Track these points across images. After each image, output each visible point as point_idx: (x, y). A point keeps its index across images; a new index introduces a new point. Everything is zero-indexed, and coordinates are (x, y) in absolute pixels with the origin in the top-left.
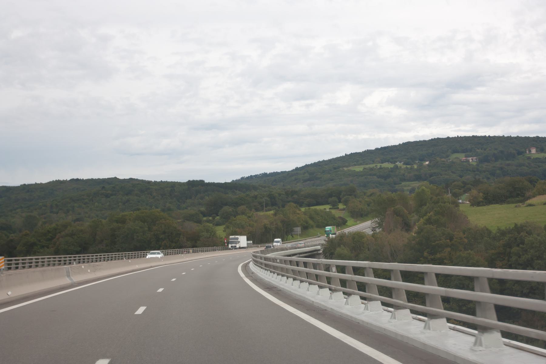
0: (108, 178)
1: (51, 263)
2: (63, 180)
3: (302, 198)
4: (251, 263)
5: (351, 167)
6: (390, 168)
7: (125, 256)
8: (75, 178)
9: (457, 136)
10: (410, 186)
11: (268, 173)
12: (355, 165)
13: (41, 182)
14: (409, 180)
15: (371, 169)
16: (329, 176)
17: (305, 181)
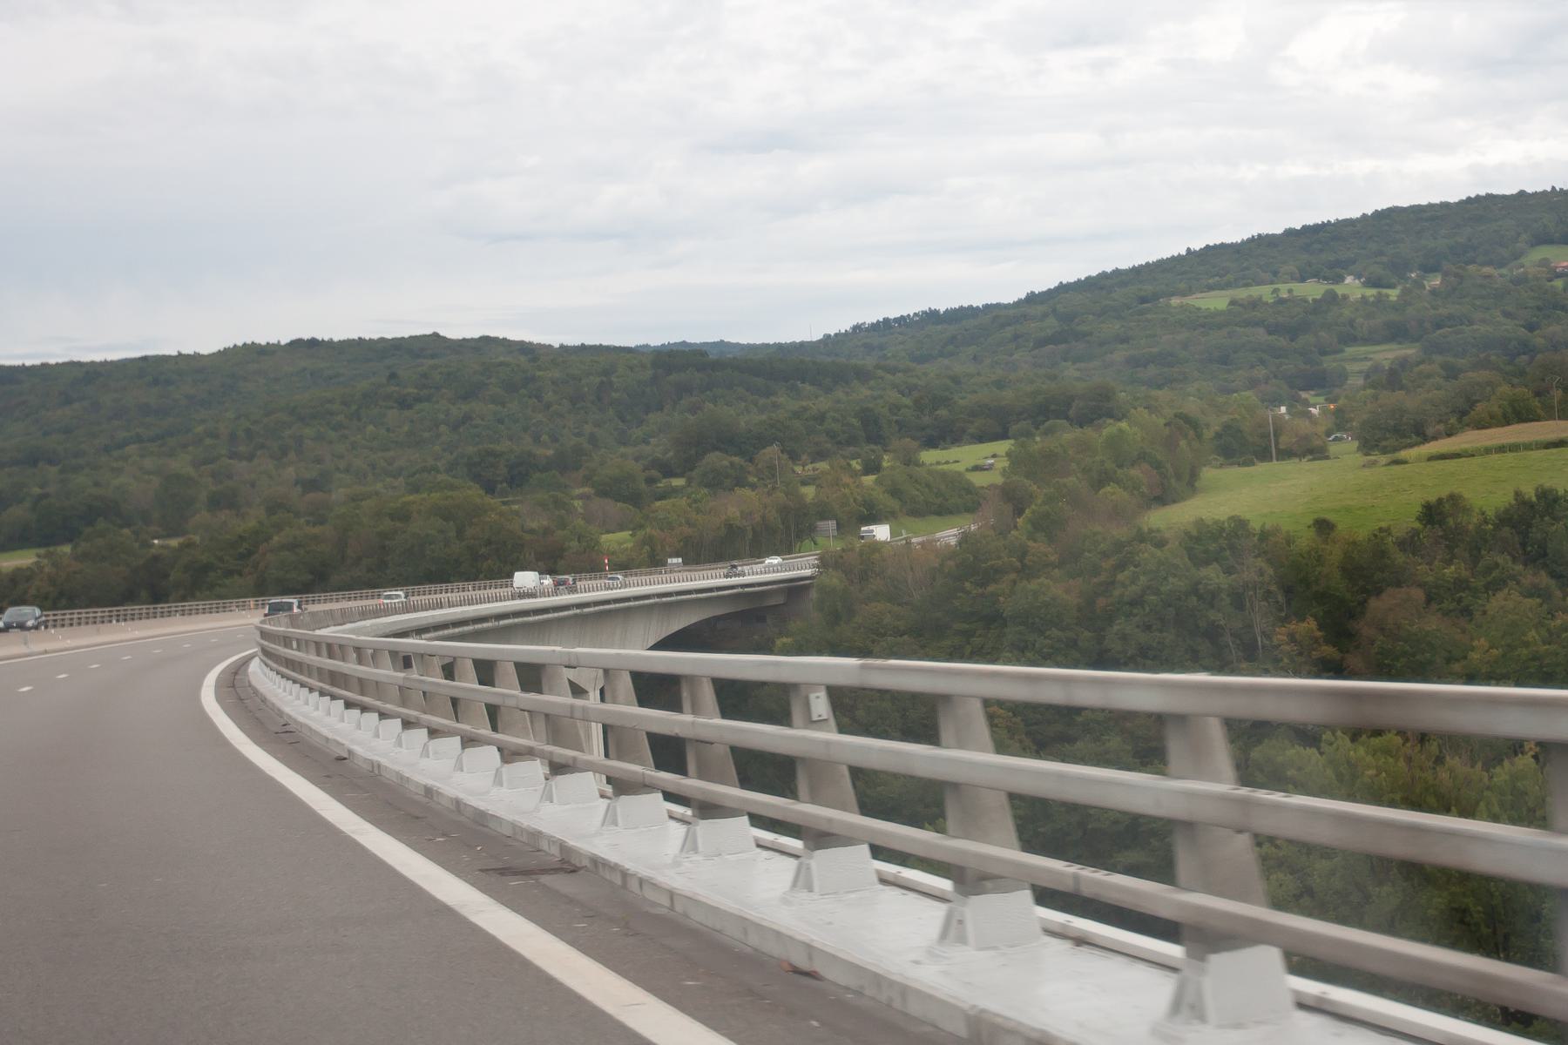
0: (411, 337)
2: (268, 343)
3: (962, 416)
5: (1194, 296)
6: (1310, 299)
8: (306, 336)
9: (1549, 189)
10: (1371, 359)
11: (942, 310)
12: (1210, 288)
13: (197, 351)
14: (1367, 341)
15: (1255, 304)
16: (1117, 327)
17: (1041, 343)
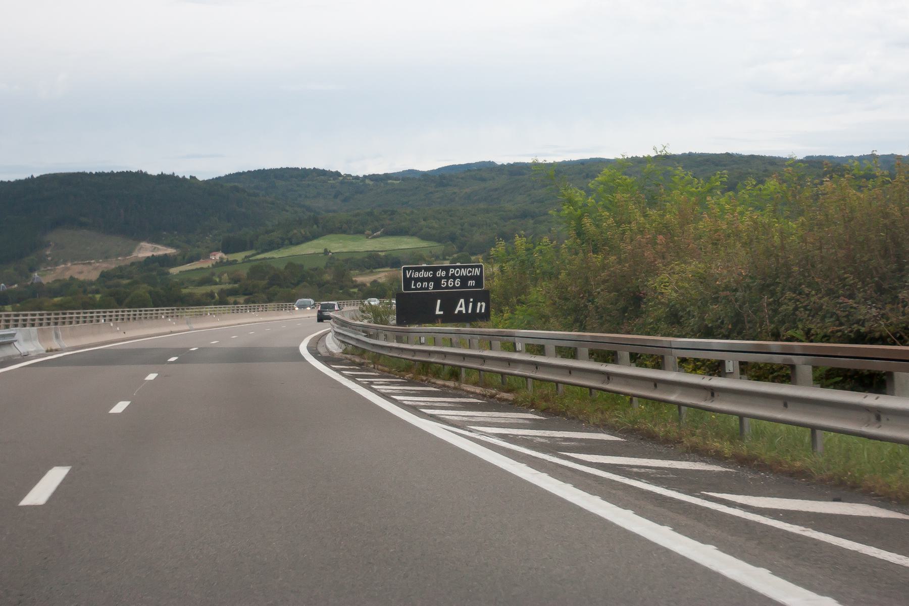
1: (60, 320)
4: (330, 336)
7: (105, 316)
